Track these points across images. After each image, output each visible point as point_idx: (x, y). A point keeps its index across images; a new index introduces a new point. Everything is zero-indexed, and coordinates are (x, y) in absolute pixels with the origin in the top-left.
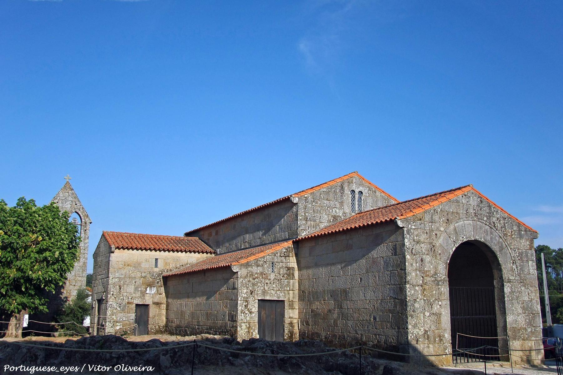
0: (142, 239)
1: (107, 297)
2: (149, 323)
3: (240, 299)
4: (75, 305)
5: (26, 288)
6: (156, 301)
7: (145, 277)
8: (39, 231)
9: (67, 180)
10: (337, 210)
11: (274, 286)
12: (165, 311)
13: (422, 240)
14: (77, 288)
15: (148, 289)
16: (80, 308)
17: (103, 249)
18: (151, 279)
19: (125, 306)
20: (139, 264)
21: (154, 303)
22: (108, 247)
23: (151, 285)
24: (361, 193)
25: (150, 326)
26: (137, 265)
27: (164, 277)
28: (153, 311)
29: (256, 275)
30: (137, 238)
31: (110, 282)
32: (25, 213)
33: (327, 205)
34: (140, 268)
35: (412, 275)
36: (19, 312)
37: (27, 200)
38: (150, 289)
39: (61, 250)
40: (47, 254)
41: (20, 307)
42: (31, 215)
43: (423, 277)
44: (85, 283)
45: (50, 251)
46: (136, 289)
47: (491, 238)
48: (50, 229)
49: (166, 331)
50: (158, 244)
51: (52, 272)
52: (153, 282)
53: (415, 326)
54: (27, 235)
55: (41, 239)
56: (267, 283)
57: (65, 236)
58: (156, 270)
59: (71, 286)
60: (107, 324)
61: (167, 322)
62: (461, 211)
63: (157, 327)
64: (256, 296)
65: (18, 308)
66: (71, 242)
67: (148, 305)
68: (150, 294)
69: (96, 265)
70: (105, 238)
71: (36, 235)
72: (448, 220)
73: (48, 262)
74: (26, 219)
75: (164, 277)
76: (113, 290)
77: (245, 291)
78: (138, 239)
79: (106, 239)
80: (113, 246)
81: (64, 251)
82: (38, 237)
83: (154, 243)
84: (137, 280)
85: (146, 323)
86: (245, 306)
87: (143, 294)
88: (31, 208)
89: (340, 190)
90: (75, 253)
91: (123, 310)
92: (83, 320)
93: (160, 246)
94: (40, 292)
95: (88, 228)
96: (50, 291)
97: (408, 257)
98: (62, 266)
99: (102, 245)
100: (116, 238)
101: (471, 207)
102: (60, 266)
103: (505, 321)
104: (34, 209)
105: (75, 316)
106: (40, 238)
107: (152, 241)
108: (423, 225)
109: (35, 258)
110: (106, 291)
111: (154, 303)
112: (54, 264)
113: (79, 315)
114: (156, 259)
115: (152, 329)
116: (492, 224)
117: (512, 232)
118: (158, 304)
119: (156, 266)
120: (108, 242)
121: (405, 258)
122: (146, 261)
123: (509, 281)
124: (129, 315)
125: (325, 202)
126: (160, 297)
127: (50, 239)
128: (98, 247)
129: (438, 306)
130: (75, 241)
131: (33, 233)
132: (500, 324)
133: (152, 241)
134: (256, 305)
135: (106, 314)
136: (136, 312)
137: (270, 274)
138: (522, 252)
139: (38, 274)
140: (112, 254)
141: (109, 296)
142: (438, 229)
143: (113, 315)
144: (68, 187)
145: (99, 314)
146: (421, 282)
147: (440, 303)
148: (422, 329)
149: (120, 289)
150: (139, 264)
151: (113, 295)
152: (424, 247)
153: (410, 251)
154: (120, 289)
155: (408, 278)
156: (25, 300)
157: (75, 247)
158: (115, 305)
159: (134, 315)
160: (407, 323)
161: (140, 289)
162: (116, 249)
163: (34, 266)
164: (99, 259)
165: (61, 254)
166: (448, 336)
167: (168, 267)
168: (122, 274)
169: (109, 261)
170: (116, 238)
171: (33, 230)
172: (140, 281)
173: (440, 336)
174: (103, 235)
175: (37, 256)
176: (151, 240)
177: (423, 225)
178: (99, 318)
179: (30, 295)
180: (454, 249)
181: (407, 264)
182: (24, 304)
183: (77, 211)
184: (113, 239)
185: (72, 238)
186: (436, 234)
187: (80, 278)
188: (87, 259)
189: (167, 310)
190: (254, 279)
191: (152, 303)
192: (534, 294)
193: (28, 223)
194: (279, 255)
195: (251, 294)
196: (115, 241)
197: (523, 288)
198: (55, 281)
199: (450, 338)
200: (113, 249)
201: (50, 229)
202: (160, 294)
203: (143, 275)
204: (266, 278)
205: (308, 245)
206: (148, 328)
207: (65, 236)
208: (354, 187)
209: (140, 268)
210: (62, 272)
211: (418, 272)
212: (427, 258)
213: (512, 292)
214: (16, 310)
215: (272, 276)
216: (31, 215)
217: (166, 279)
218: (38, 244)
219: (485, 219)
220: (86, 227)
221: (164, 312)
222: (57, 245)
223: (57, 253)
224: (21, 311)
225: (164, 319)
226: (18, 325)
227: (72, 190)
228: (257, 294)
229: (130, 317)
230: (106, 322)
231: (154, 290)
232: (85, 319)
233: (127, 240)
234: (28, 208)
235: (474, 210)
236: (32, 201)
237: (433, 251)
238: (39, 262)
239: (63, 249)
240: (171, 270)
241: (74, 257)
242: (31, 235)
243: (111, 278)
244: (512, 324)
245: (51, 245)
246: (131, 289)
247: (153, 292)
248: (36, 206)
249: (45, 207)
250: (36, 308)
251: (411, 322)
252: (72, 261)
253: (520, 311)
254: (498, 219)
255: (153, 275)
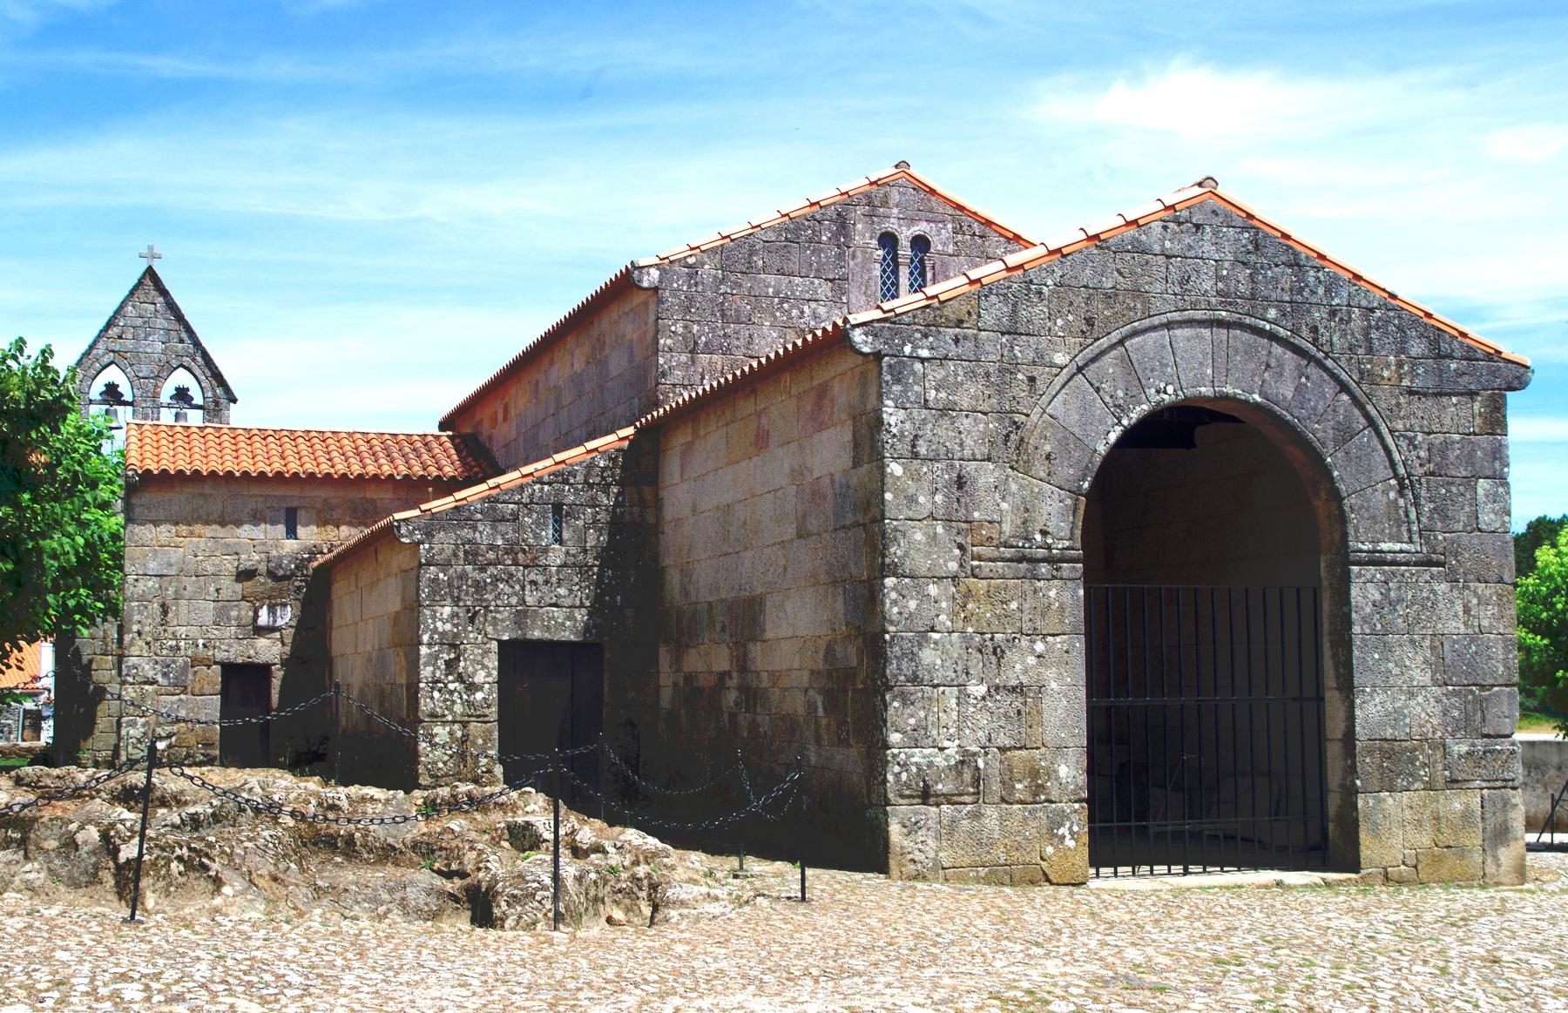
3: (425, 638)
10: (822, 310)
11: (562, 591)
13: (965, 403)
19: (184, 669)
24: (921, 243)
29: (491, 555)
33: (776, 294)
35: (918, 541)
43: (961, 547)
47: (1299, 389)
53: (917, 738)
56: (533, 583)
62: (1159, 287)
64: (489, 629)
72: (1089, 322)
77: (447, 611)
86: (448, 663)
89: (836, 235)
97: (895, 468)
101: (1208, 269)
103: (1351, 718)
108: (969, 345)
116: (1305, 332)
117: (1400, 365)
121: (883, 474)
123: (1376, 560)
125: (771, 279)
129: (1031, 660)
132: (1335, 728)
134: (493, 662)
137: (545, 550)
138: (1446, 445)
141: (127, 638)
142: (1040, 359)
146: (953, 566)
147: (1040, 647)
148: (952, 748)
149: (165, 612)
151: (139, 633)
152: (973, 432)
153: (903, 448)
154: (165, 612)
155: (895, 551)
160: (885, 721)
161: (234, 613)
166: (1070, 772)
173: (1034, 773)
177: (969, 345)
180: (1113, 437)
181: (888, 496)
186: (1032, 379)
190: (483, 569)
192: (1492, 610)
194: (580, 478)
195: (472, 620)
197: (1442, 587)
199: (1082, 779)
204: (532, 565)
205: (713, 438)
208: (892, 225)
211: (940, 530)
212: (986, 475)
213: (1387, 604)
215: (556, 556)
219: (1272, 313)
228: (495, 622)
235: (1219, 278)
237: (1012, 445)
244: (1382, 725)
251: (900, 720)
253: (1422, 677)
254: (1333, 314)
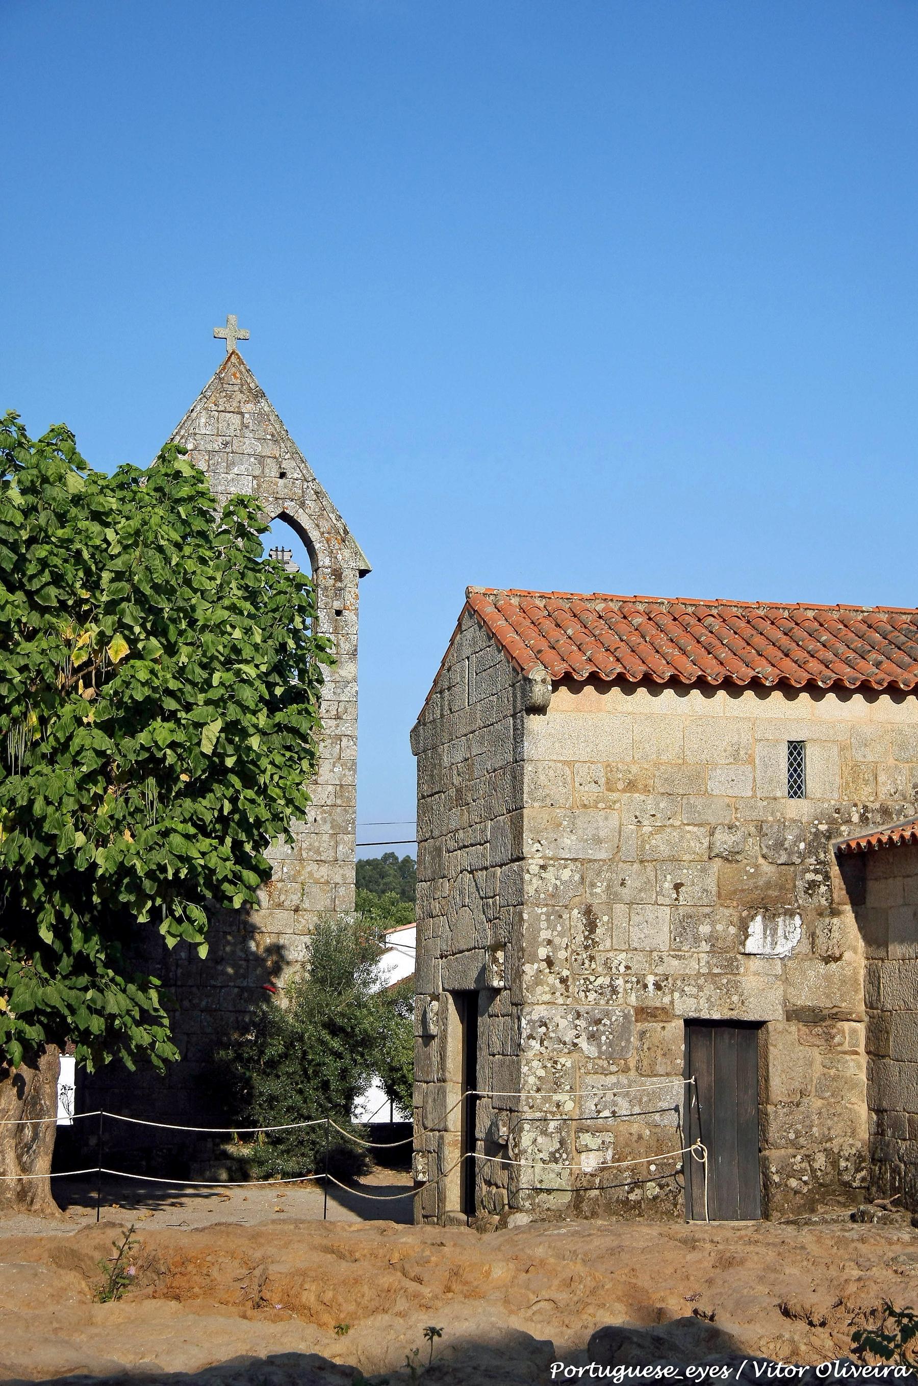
0: (699, 630)
1: (519, 974)
2: (773, 1133)
4: (310, 1012)
5: (61, 929)
6: (804, 999)
7: (731, 857)
8: (111, 607)
9: (231, 346)
12: (863, 1059)
14: (309, 920)
15: (756, 926)
16: (333, 1029)
17: (474, 695)
18: (767, 869)
19: (625, 1029)
20: (697, 777)
21: (794, 1014)
22: (504, 677)
23: (769, 905)
25: (774, 1155)
26: (682, 785)
27: (845, 857)
28: (789, 1060)
30: (667, 621)
31: (530, 890)
32: (28, 512)
34: (698, 802)
36: (32, 1055)
37: (35, 434)
38: (770, 930)
39: (233, 712)
40: (160, 732)
41: (34, 1033)
42: (62, 519)
44: (348, 894)
45: (171, 716)
46: (684, 927)
48: (167, 590)
49: (874, 1187)
50: (800, 655)
51: (187, 837)
52: (784, 887)
54: (50, 630)
55: (125, 650)
57: (248, 631)
58: (797, 809)
59: (280, 914)
60: (526, 1140)
61: (879, 1131)
63: (820, 1161)
65: (21, 1037)
66: (279, 669)
67: (759, 1025)
68: (769, 958)
69: (432, 788)
70: (483, 624)
71: (91, 632)
73: (166, 777)
74: (31, 541)
75: (845, 857)
76: (549, 935)
78: (676, 631)
79: (492, 636)
80: (537, 674)
81: (247, 720)
82: (103, 640)
83: (771, 651)
84: (686, 875)
85: (752, 1135)
87: (730, 956)
88: (61, 478)
90: (304, 727)
91: (614, 1054)
92: (350, 1093)
93: (814, 666)
94: (133, 950)
95: (349, 598)
96: (183, 944)
98: (244, 792)
99: (464, 672)
100: (548, 625)
102: (234, 800)
104: (76, 483)
105: (309, 1071)
106: (118, 649)
107: (758, 640)
109: (100, 754)
110: (508, 941)
111: (794, 1014)
112: (197, 790)
113: (331, 1069)
114: (796, 748)
115: (788, 1172)
118: (816, 1019)
119: (796, 788)
120: (502, 647)
122: (738, 756)
124: (652, 1084)
126: (828, 978)
127: (171, 650)
128: (441, 687)
130: (301, 659)
131: (82, 619)
133: (758, 640)
135: (514, 1081)
136: (688, 1072)
139: (120, 842)
140: (534, 722)
141: (530, 970)
143: (557, 1085)
144: (232, 378)
145: (470, 1079)
149: (591, 926)
150: (697, 777)
151: (550, 962)
154: (591, 926)
156: (55, 993)
157: (296, 696)
158: (564, 1026)
159: (678, 1085)
161: (704, 929)
162: (556, 685)
163: (98, 799)
164: (452, 756)
165: (232, 729)
167: (865, 795)
168: (598, 841)
169: (518, 760)
170: (548, 625)
171: (80, 602)
172: (703, 883)
174: (470, 610)
175: (104, 742)
176: (748, 631)
178: (470, 1106)
179: (83, 965)
182: (55, 1013)
183: (291, 508)
184: (533, 633)
185: (283, 647)
187: (323, 872)
188: (353, 766)
189: (877, 1052)
191: (779, 1014)
193: (44, 563)
196: (544, 646)
198: (209, 884)
200: (539, 692)
201: (167, 590)
202: (829, 959)
203: (724, 840)
206: (764, 1164)
207: (248, 631)
209: (698, 802)
210: (247, 835)
214: (16, 1049)
216: (62, 519)
217: (860, 866)
218: (110, 676)
220: (339, 592)
221: (857, 1068)
222: (208, 683)
223: (214, 729)
224: (41, 1050)
225: (862, 1111)
226: (28, 1133)
227: (258, 395)
229: (654, 1095)
230: (516, 1130)
231: (791, 935)
232: (359, 1091)
233: (612, 639)
234: (45, 480)
236: (63, 435)
238: (121, 779)
239: (245, 709)
240: (885, 812)
241: (299, 747)
242: (66, 626)
243: (533, 865)
245: (173, 685)
246: (654, 927)
247: (783, 948)
248: (81, 467)
249: (126, 481)
250: (114, 1037)
252: (295, 776)
255: (779, 844)
